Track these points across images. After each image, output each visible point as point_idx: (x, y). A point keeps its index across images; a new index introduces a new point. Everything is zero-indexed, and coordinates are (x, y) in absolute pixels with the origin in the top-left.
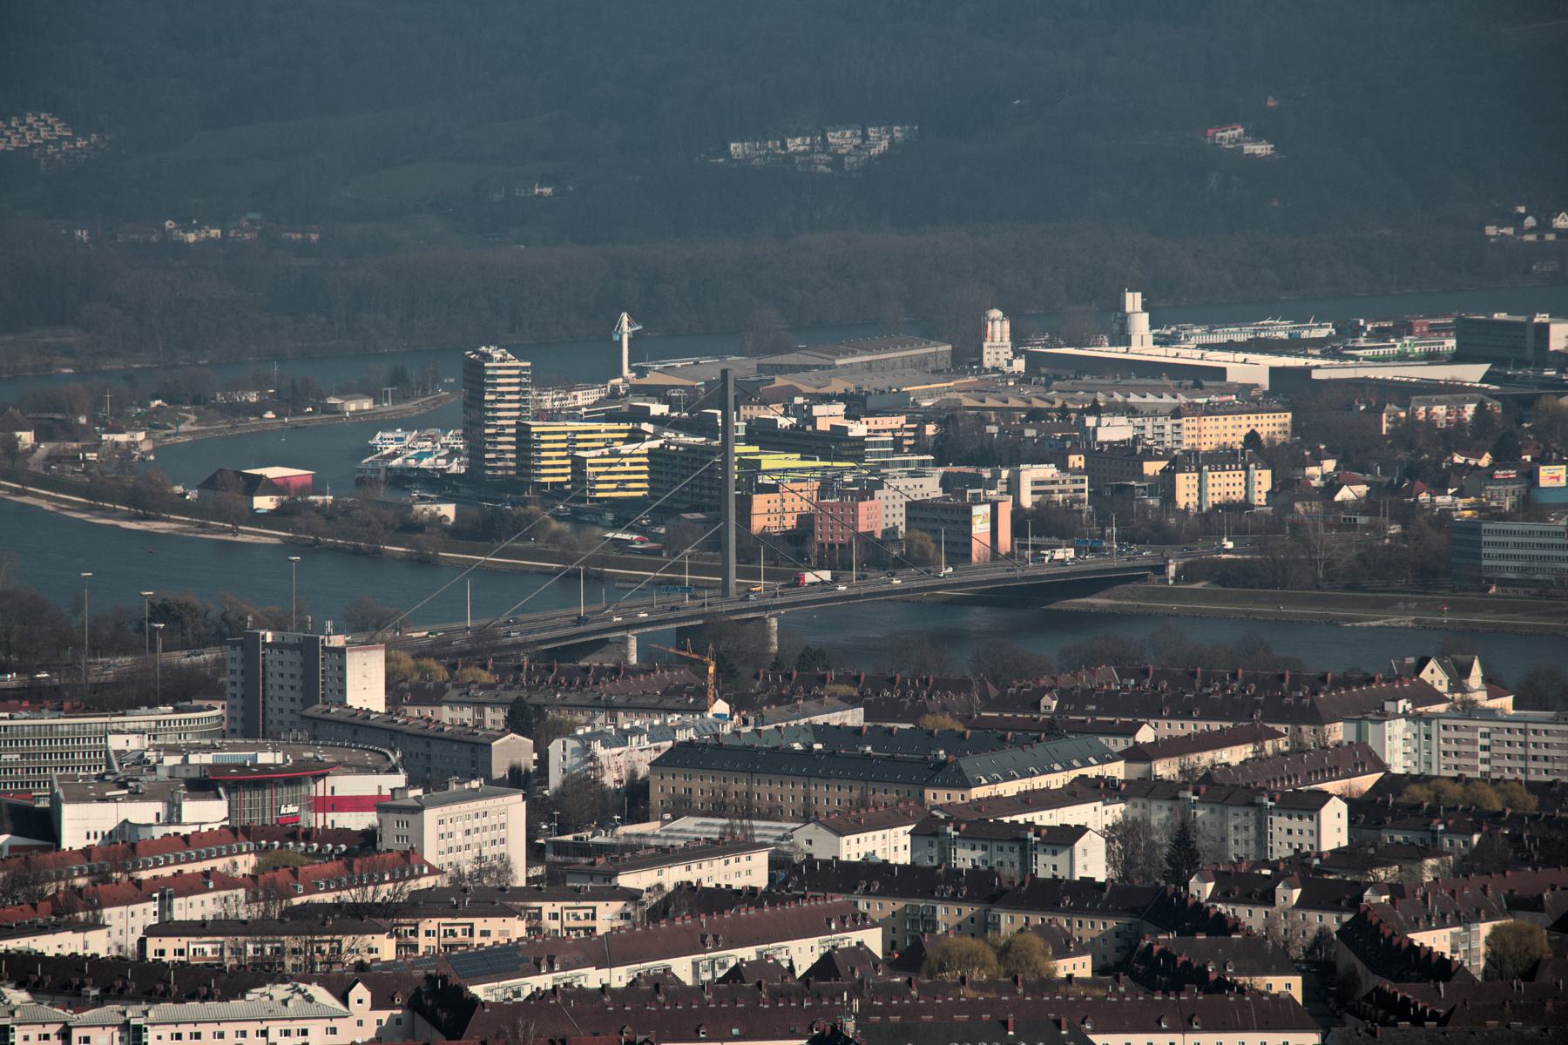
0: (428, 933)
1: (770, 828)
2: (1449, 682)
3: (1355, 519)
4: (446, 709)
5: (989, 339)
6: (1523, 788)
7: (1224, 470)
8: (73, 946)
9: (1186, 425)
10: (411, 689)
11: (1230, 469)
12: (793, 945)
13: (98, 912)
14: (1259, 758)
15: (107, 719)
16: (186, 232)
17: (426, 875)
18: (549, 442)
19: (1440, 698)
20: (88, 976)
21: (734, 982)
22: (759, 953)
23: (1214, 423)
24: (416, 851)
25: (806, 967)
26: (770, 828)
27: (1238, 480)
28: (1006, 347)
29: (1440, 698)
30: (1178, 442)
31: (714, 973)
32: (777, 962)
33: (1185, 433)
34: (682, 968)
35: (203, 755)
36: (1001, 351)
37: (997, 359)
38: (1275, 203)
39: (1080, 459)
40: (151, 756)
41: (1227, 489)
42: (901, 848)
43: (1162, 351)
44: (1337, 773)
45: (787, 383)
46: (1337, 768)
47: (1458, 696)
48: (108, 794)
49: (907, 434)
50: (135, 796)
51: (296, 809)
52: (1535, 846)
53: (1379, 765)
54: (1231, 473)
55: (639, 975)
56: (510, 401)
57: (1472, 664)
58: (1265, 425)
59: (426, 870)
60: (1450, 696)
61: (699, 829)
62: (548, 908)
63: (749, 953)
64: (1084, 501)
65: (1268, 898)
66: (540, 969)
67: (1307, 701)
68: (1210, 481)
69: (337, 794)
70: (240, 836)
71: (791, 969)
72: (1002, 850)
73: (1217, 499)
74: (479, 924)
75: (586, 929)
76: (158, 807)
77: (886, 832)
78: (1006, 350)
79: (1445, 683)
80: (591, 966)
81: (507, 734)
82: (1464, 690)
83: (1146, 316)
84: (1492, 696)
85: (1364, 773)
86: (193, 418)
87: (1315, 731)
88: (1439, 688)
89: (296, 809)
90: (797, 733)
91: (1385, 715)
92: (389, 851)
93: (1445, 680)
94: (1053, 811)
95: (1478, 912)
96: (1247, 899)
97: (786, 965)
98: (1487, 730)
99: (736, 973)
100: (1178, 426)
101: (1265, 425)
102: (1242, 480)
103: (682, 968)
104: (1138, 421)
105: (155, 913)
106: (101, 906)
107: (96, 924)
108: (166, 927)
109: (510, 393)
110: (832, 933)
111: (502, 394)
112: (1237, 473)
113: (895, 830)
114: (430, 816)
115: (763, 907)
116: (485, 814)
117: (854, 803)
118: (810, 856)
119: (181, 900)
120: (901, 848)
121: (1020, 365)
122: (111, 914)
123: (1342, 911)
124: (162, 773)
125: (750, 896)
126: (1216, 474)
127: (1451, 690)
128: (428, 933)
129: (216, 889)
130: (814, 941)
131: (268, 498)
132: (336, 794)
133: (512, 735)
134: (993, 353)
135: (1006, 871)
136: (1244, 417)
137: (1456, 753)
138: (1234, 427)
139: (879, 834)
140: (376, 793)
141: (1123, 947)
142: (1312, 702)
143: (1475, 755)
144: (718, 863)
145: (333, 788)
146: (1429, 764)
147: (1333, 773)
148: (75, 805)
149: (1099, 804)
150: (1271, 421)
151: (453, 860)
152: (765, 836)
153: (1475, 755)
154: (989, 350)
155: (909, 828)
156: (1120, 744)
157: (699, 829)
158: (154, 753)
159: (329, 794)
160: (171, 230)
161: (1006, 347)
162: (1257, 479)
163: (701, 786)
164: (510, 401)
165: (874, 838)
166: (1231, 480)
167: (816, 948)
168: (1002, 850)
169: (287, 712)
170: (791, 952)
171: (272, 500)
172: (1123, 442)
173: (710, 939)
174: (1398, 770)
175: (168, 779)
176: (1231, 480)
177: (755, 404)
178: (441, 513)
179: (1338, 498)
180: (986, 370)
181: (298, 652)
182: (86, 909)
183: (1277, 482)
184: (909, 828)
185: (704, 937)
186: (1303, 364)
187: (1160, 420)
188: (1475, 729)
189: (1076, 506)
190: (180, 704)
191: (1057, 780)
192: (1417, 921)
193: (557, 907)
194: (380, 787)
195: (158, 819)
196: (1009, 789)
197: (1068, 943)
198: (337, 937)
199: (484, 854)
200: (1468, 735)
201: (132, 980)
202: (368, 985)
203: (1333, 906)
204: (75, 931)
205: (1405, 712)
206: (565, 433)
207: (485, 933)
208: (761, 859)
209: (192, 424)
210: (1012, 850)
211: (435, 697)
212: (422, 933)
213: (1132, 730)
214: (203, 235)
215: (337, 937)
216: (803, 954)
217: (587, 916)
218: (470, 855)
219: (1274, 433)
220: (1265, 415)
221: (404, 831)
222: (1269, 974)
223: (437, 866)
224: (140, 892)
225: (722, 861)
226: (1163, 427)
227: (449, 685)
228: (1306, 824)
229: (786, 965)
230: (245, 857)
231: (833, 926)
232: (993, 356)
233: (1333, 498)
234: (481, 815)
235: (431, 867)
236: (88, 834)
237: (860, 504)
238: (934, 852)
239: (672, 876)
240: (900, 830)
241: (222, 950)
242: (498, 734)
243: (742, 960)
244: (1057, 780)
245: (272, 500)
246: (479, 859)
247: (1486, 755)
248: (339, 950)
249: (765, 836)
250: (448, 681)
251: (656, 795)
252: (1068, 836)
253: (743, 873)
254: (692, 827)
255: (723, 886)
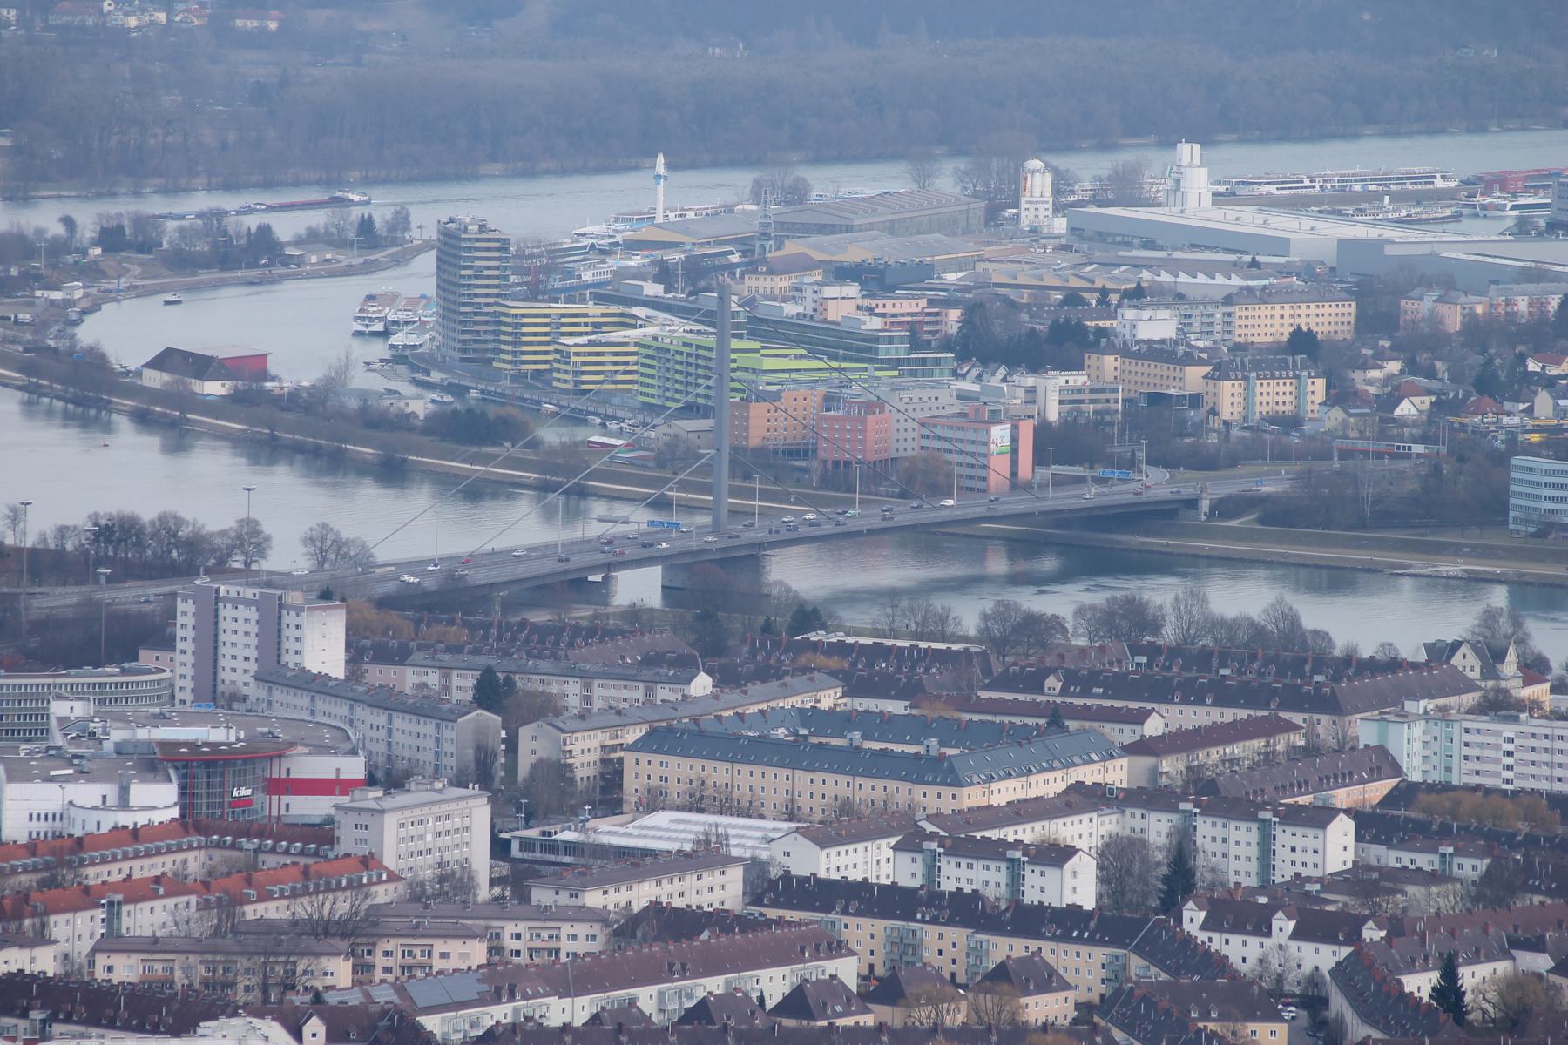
0: (386, 954)
1: (750, 828)
2: (1482, 668)
3: (1410, 448)
4: (409, 671)
5: (1028, 194)
6: (1544, 802)
7: (1273, 377)
8: (19, 962)
9: (1238, 313)
10: (373, 647)
11: (1281, 378)
12: (764, 974)
13: (45, 919)
14: (1269, 757)
15: (50, 681)
16: (127, 14)
17: (385, 882)
18: (531, 344)
19: (1470, 687)
20: (36, 998)
21: (700, 1023)
22: (727, 983)
23: (1269, 312)
24: (376, 856)
25: (778, 998)
26: (750, 828)
27: (1288, 389)
28: (1047, 202)
29: (1470, 687)
30: (1229, 332)
31: (681, 1004)
32: (746, 994)
33: (1238, 322)
34: (646, 998)
35: (153, 730)
36: (1042, 207)
37: (1037, 216)
38: (1367, 17)
39: (1116, 360)
40: (95, 726)
41: (1277, 399)
42: (883, 861)
43: (1218, 213)
44: (1351, 778)
45: (801, 250)
46: (1350, 773)
47: (1490, 684)
48: (53, 773)
49: (927, 319)
50: (83, 774)
51: (249, 792)
52: (1547, 872)
53: (1396, 769)
54: (1281, 382)
55: (602, 1008)
56: (488, 277)
57: (1507, 649)
58: (1327, 315)
59: (384, 877)
60: (1482, 684)
61: (674, 826)
62: (510, 928)
63: (714, 985)
64: (1116, 411)
65: (1263, 929)
66: (500, 998)
67: (1327, 690)
68: (1258, 389)
69: (292, 776)
70: (191, 830)
71: (762, 1000)
72: (988, 869)
73: (1265, 409)
74: (439, 946)
75: (550, 952)
76: (110, 790)
77: (869, 844)
78: (1046, 206)
79: (1477, 669)
80: (554, 995)
81: (475, 710)
82: (1496, 676)
83: (1204, 171)
84: (1527, 682)
85: (1381, 779)
86: (137, 270)
87: (1334, 723)
88: (1469, 673)
89: (249, 792)
90: (782, 717)
91: (1405, 716)
92: (347, 855)
93: (1478, 665)
94: (1046, 823)
95: (1477, 951)
96: (1238, 928)
97: (754, 996)
98: (1511, 735)
99: (701, 1012)
100: (1230, 314)
101: (1327, 315)
102: (1293, 389)
103: (646, 998)
104: (1185, 309)
105: (103, 920)
106: (47, 913)
107: (41, 938)
108: (113, 941)
109: (488, 268)
110: (804, 961)
111: (479, 268)
112: (1288, 381)
113: (878, 842)
114: (390, 821)
115: (734, 933)
116: (448, 817)
117: (839, 801)
118: (787, 872)
119: (130, 907)
120: (883, 861)
121: (1060, 225)
122: (60, 925)
123: (1340, 943)
124: (108, 746)
125: (720, 920)
126: (1265, 382)
127: (1484, 677)
128: (386, 954)
129: (168, 895)
130: (786, 970)
131: (220, 383)
132: (292, 776)
133: (480, 711)
134: (1032, 210)
135: (990, 893)
136: (1303, 306)
137: (1478, 758)
138: (1292, 316)
139: (860, 846)
140: (334, 777)
141: (1109, 980)
142: (1333, 692)
143: (1497, 761)
144: (690, 880)
145: (288, 770)
146: (1448, 770)
147: (1345, 778)
148: (18, 785)
149: (1094, 815)
150: (1334, 310)
151: (413, 865)
152: (742, 837)
153: (1497, 761)
154: (1027, 206)
155: (893, 841)
156: (1124, 734)
157: (674, 826)
158: (100, 725)
159: (284, 775)
160: (109, 12)
161: (1047, 202)
162: (1310, 388)
163: (680, 770)
164: (488, 277)
165: (856, 851)
166: (1281, 389)
167: (787, 978)
168: (988, 869)
169: (240, 671)
170: (761, 981)
171: (223, 385)
172: (1162, 341)
173: (678, 966)
174: (1416, 777)
175: (115, 756)
176: (1281, 389)
177: (762, 273)
178: (409, 410)
179: (1398, 412)
180: (1023, 232)
181: (254, 609)
182: (33, 915)
183: (1333, 392)
184: (893, 841)
185: (671, 965)
186: (1376, 236)
187: (1210, 310)
188: (1499, 733)
189: (1107, 418)
190: (126, 665)
191: (1050, 784)
192: (1413, 960)
193: (522, 927)
194: (338, 770)
195: (104, 801)
196: (1004, 792)
197: (1050, 976)
198: (292, 959)
199: (445, 860)
200: (1492, 740)
201: (81, 1003)
202: (322, 1017)
203: (1329, 938)
204: (22, 946)
205: (1426, 712)
206: (546, 316)
207: (444, 955)
208: (735, 875)
209: (135, 277)
210: (998, 869)
211: (399, 656)
212: (379, 953)
213: (1140, 717)
214: (147, 18)
215: (292, 959)
216: (774, 984)
217: (551, 937)
218: (431, 859)
219: (1336, 332)
220: (1327, 305)
221: (360, 833)
222: (1254, 1019)
223: (396, 872)
224: (87, 898)
225: (695, 876)
226: (1212, 315)
227: (413, 644)
228: (1311, 843)
229: (754, 996)
230: (196, 853)
231: (807, 955)
232: (1032, 213)
233: (1392, 411)
234: (443, 818)
235: (390, 873)
236: (31, 815)
237: (870, 418)
238: (919, 868)
239: (641, 895)
240: (883, 843)
241: (172, 969)
242: (464, 710)
243: (710, 993)
244: (1050, 784)
245: (223, 385)
246: (440, 865)
247: (1508, 760)
248: (294, 972)
249: (742, 837)
250: (413, 640)
251: (632, 784)
252: (1057, 855)
253: (716, 889)
254: (666, 825)
255: (694, 907)
